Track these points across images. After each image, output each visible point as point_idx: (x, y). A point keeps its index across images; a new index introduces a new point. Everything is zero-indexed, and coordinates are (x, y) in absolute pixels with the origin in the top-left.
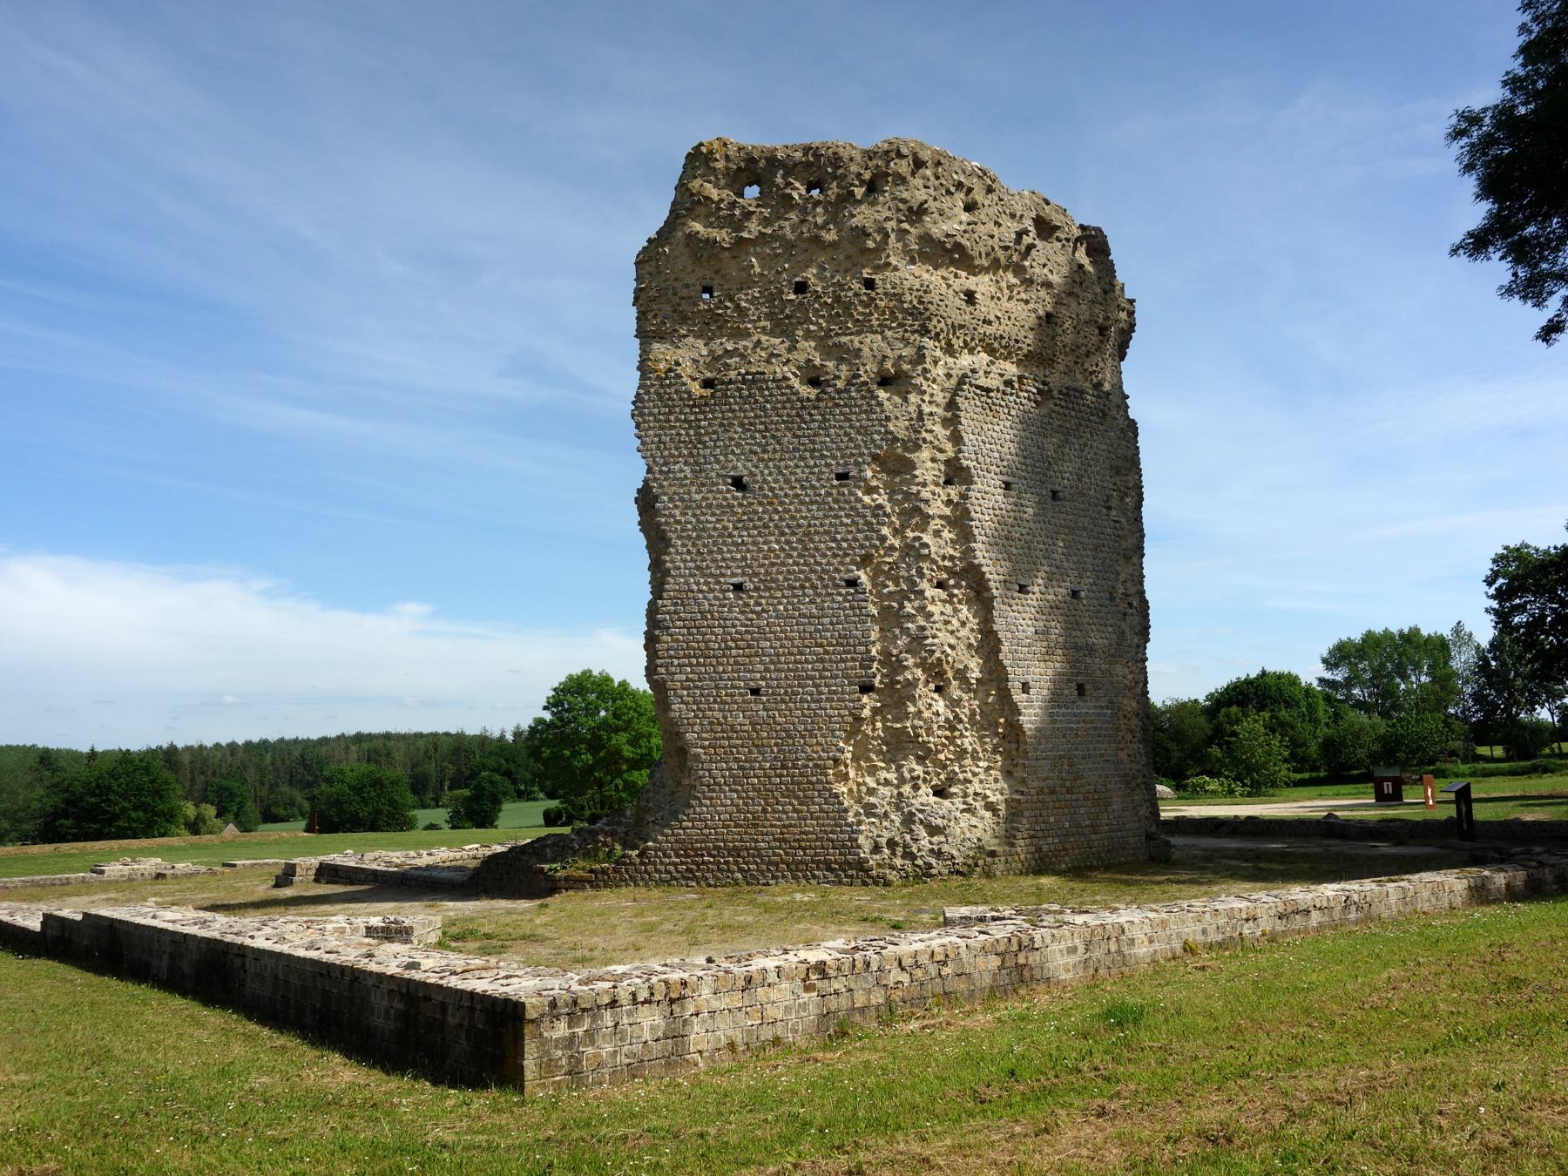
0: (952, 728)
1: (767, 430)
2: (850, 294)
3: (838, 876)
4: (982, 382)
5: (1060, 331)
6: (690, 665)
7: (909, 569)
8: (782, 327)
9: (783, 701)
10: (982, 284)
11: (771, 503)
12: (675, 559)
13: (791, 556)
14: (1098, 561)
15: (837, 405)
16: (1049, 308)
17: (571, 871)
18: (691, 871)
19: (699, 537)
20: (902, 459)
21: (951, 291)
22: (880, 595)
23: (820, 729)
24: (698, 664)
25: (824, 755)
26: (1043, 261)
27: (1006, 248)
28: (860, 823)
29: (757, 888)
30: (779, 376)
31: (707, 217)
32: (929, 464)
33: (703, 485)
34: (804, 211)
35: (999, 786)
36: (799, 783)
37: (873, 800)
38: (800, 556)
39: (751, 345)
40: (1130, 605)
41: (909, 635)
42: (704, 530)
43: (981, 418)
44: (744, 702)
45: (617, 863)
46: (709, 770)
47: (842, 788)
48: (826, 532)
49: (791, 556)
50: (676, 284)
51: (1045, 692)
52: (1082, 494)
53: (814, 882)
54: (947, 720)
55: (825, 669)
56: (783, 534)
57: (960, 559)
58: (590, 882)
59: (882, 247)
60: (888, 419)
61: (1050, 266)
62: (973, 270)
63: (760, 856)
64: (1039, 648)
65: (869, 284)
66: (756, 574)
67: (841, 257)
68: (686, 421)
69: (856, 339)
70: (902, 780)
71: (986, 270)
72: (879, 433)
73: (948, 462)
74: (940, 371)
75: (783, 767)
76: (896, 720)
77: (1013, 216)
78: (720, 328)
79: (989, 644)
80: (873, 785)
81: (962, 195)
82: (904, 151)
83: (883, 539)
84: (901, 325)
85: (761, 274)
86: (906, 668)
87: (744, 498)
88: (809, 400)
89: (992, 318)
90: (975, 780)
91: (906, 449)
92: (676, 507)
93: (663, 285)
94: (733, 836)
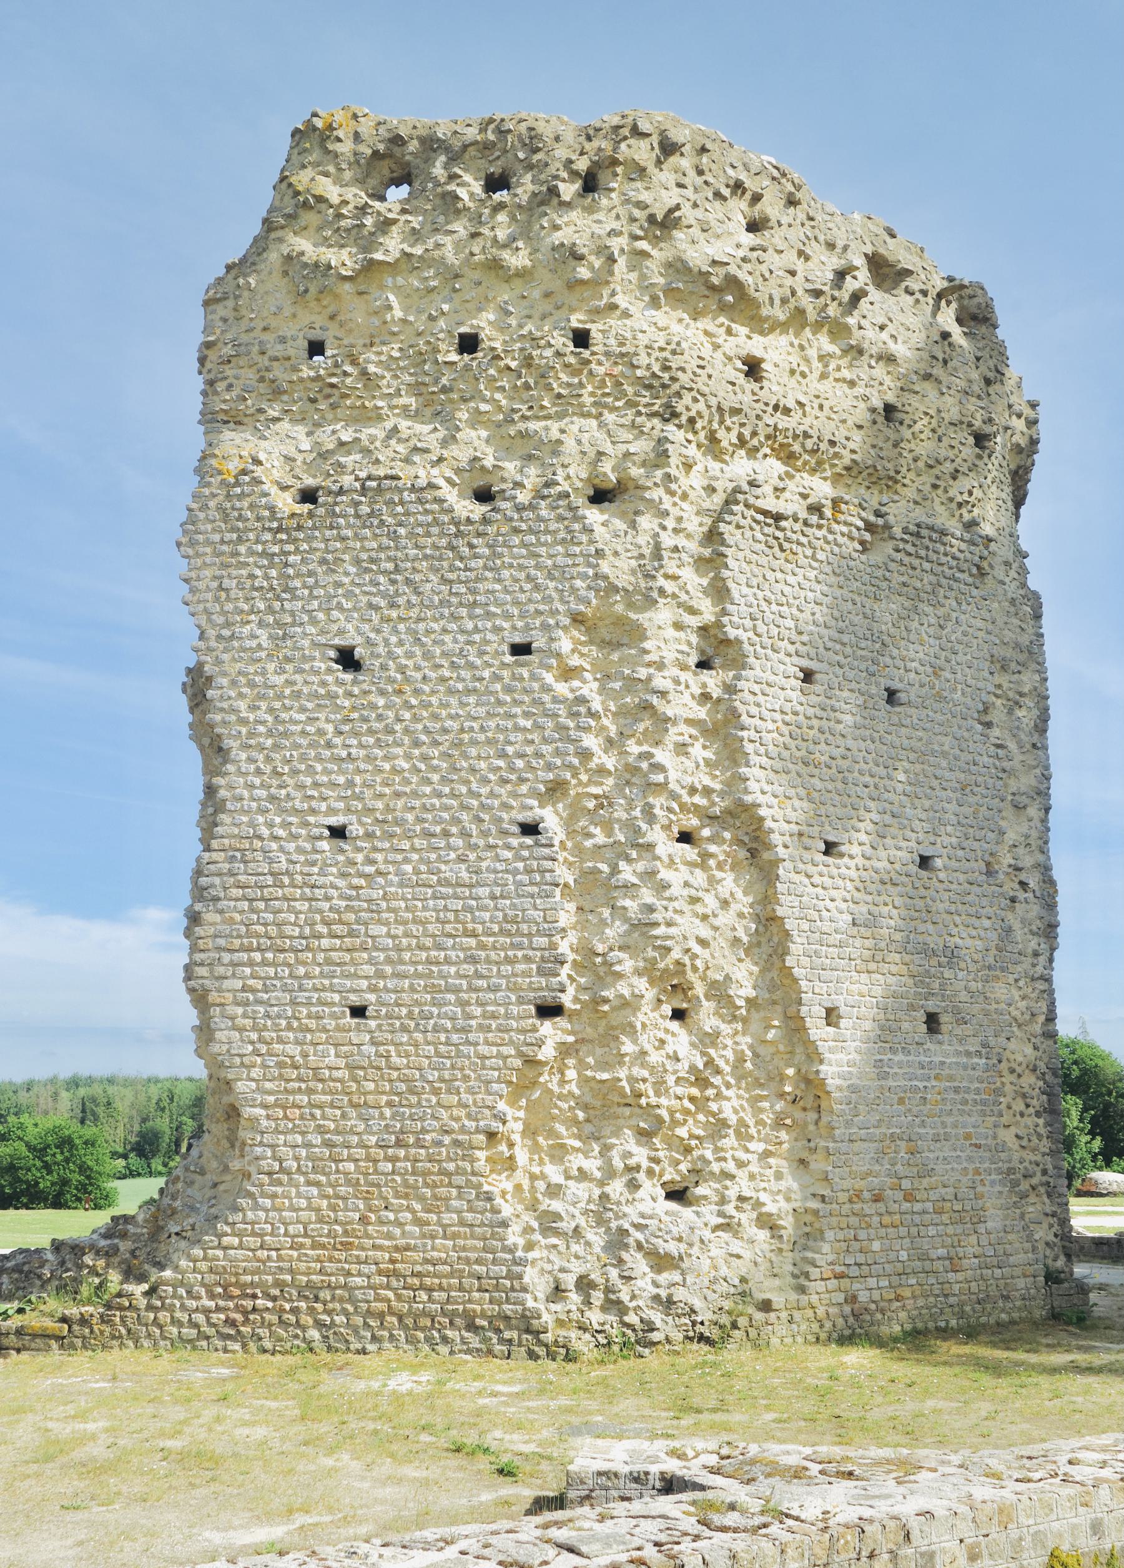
0: (702, 1082)
1: (397, 569)
2: (548, 353)
3: (486, 1340)
4: (770, 503)
5: (907, 434)
6: (251, 963)
7: (630, 808)
8: (435, 404)
9: (404, 1029)
10: (775, 350)
11: (400, 692)
12: (234, 782)
13: (428, 782)
14: (966, 810)
15: (516, 531)
16: (891, 398)
17: (33, 1320)
18: (232, 1323)
19: (276, 747)
20: (620, 622)
21: (719, 355)
22: (579, 850)
23: (466, 1078)
24: (264, 963)
25: (471, 1125)
26: (881, 320)
27: (817, 293)
28: (530, 1246)
29: (341, 1358)
30: (422, 482)
31: (320, 228)
32: (670, 632)
33: (288, 660)
34: (478, 219)
35: (783, 1185)
36: (426, 1173)
37: (556, 1206)
38: (444, 780)
39: (381, 435)
40: (1023, 885)
41: (626, 920)
42: (285, 734)
43: (763, 560)
44: (338, 1029)
45: (108, 1306)
46: (273, 1147)
47: (499, 1184)
48: (489, 742)
49: (428, 782)
50: (266, 337)
51: (868, 1025)
52: (940, 698)
53: (444, 1349)
54: (693, 1069)
55: (479, 976)
56: (417, 744)
57: (722, 794)
58: (60, 1338)
59: (599, 282)
60: (599, 553)
61: (891, 328)
62: (760, 325)
63: (352, 1300)
64: (858, 948)
65: (581, 339)
66: (371, 811)
67: (536, 294)
68: (264, 554)
69: (555, 426)
70: (610, 1173)
71: (782, 327)
72: (584, 576)
73: (703, 630)
74: (695, 481)
75: (399, 1144)
76: (604, 1065)
77: (831, 246)
78: (334, 407)
79: (769, 936)
80: (556, 1178)
81: (744, 205)
82: (644, 126)
83: (585, 755)
84: (631, 404)
85: (404, 321)
86: (619, 976)
87: (355, 682)
88: (469, 521)
89: (791, 404)
90: (742, 1174)
91: (631, 605)
92: (241, 695)
93: (244, 338)
94: (307, 1266)
